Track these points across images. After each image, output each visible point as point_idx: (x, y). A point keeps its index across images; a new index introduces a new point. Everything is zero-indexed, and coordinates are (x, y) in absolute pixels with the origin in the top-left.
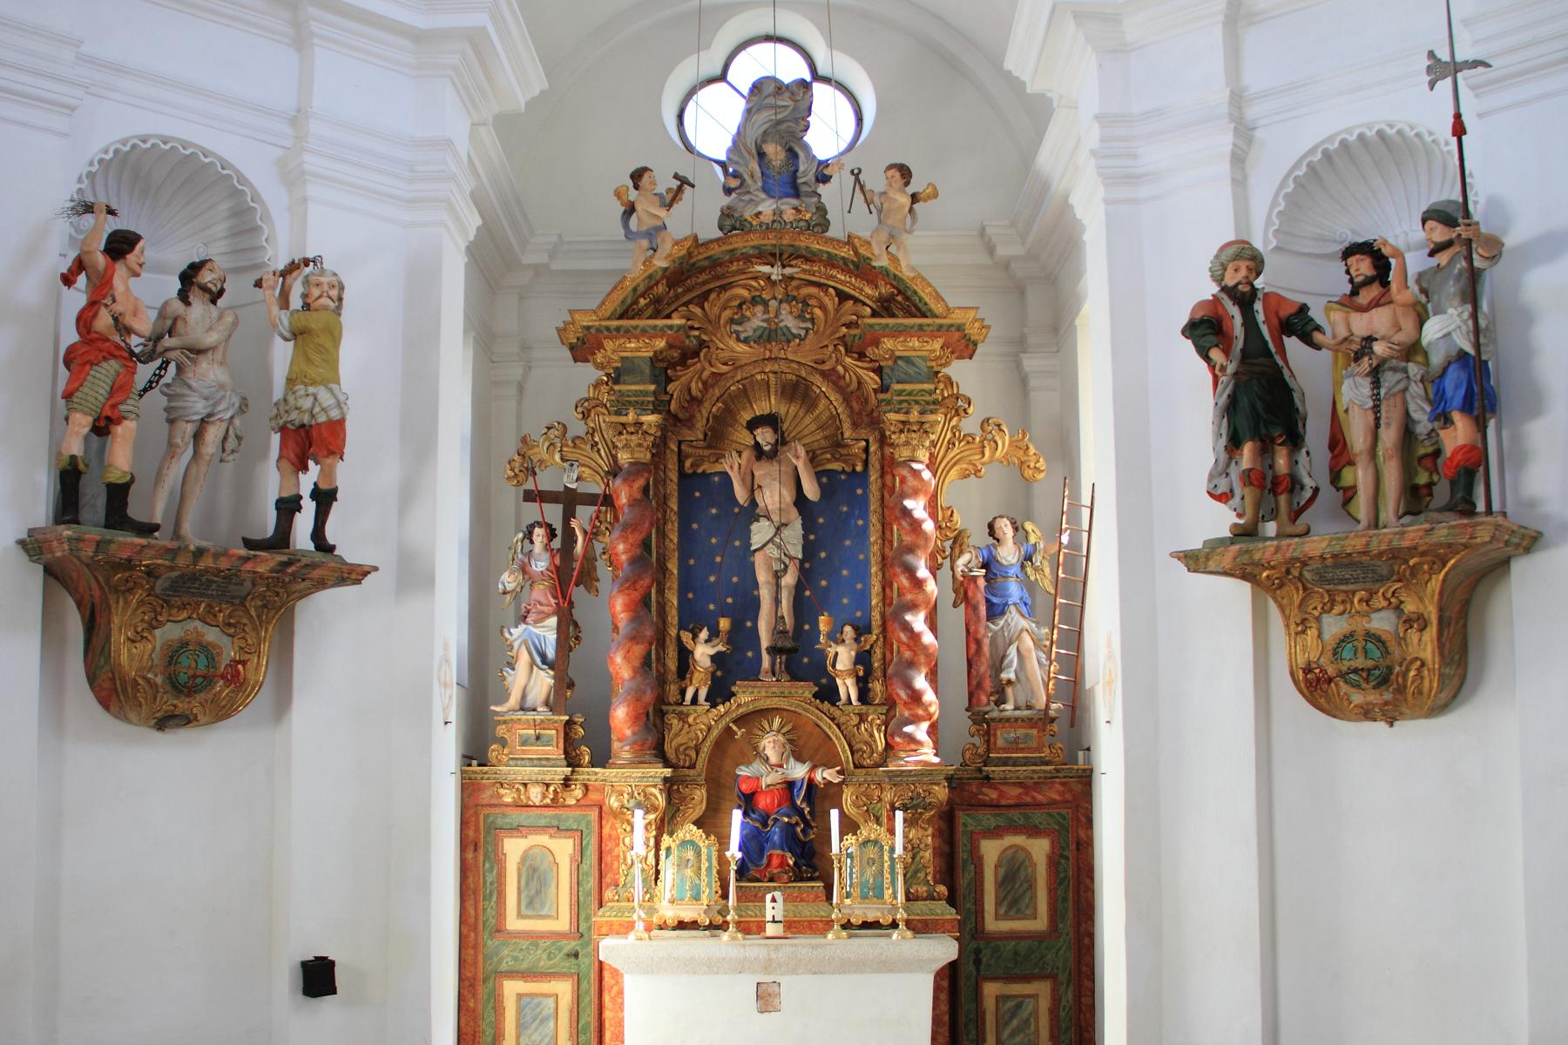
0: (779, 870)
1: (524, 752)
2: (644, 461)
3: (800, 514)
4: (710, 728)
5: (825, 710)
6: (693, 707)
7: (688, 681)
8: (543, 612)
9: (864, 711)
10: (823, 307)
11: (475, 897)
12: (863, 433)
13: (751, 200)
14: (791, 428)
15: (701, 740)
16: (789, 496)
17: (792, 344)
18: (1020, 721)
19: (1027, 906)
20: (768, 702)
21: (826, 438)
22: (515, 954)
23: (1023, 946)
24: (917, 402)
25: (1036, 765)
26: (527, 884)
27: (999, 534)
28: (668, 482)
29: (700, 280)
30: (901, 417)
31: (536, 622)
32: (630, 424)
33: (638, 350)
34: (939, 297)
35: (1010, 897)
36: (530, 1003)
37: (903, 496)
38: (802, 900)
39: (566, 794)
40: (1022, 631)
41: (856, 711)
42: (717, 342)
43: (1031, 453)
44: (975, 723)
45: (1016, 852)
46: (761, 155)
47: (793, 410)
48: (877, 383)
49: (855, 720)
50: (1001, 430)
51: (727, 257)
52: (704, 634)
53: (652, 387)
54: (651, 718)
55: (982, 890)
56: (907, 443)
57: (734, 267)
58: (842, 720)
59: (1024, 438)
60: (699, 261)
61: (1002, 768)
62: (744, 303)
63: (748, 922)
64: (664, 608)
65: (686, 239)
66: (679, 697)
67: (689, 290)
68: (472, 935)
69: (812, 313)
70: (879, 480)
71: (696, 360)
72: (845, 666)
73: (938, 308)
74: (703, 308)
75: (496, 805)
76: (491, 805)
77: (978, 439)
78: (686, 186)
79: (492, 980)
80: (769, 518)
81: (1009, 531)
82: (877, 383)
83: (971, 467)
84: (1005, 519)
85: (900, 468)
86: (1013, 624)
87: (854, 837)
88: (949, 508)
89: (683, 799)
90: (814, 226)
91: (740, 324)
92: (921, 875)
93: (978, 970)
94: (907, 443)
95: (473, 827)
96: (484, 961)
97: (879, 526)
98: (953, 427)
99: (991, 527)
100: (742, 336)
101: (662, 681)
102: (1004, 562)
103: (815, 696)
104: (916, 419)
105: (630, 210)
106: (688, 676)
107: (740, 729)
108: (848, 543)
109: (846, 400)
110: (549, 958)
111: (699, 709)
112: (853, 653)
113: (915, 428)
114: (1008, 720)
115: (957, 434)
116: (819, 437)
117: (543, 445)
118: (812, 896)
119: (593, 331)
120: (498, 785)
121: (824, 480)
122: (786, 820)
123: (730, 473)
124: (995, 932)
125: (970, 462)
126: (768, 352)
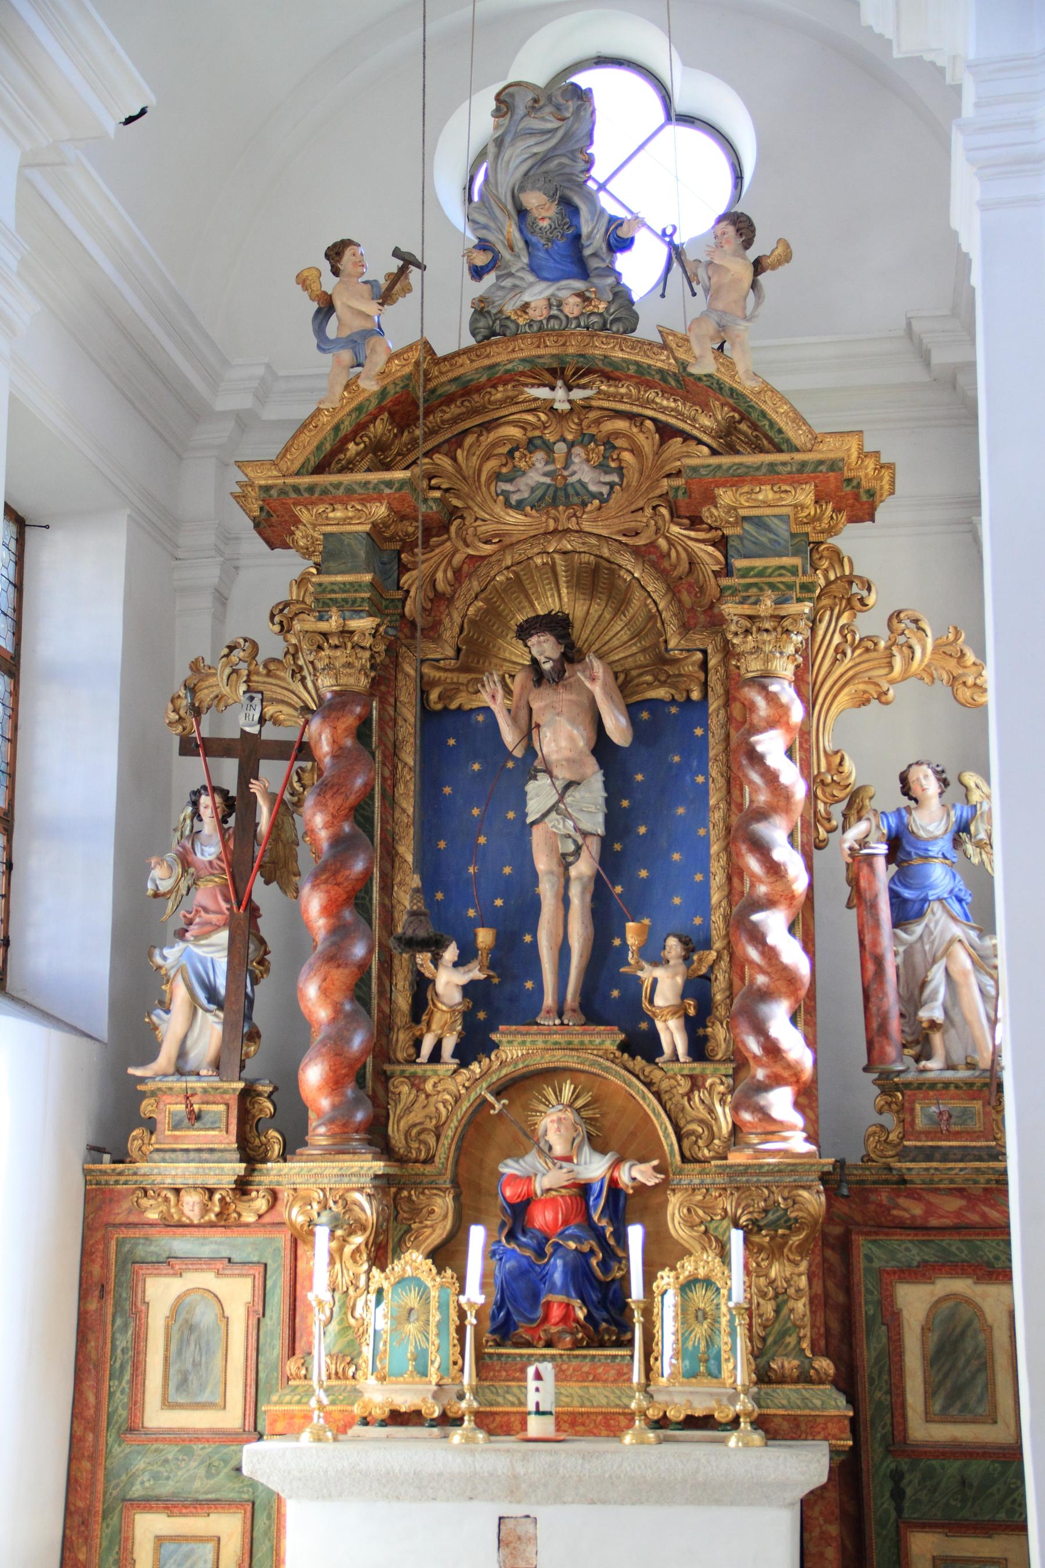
0: (560, 1328)
1: (176, 1137)
2: (356, 689)
3: (601, 767)
4: (458, 1099)
5: (637, 1070)
6: (430, 1067)
7: (423, 1026)
8: (210, 923)
9: (697, 1071)
10: (635, 450)
11: (97, 1372)
12: (698, 639)
13: (515, 286)
14: (593, 638)
15: (443, 1119)
16: (581, 739)
17: (589, 508)
18: (952, 1087)
19: (980, 1401)
20: (548, 1057)
21: (644, 650)
22: (156, 1468)
23: (976, 1469)
24: (773, 586)
25: (980, 1159)
26: (180, 1352)
27: (916, 791)
28: (400, 722)
29: (446, 416)
30: (746, 609)
31: (197, 938)
32: (331, 634)
33: (345, 521)
34: (798, 419)
35: (949, 1384)
36: (174, 1552)
37: (755, 730)
38: (596, 1379)
39: (241, 1207)
40: (951, 942)
41: (686, 1072)
42: (476, 509)
43: (969, 663)
44: (884, 1092)
45: (957, 1305)
46: (522, 213)
47: (596, 609)
48: (718, 562)
49: (685, 1085)
50: (920, 628)
51: (484, 379)
52: (451, 953)
53: (368, 577)
54: (369, 1083)
55: (901, 1370)
56: (757, 650)
57: (499, 395)
58: (665, 1085)
59: (956, 639)
60: (443, 384)
61: (924, 1165)
62: (517, 448)
63: (507, 1413)
64: (392, 913)
65: (410, 348)
66: (412, 1051)
67: (431, 433)
68: (90, 1437)
69: (619, 459)
70: (722, 712)
71: (446, 536)
72: (666, 999)
73: (797, 435)
74: (454, 459)
75: (135, 1225)
76: (129, 1225)
77: (882, 644)
78: (412, 267)
79: (117, 1512)
80: (548, 772)
81: (931, 786)
82: (718, 562)
83: (872, 690)
84: (925, 767)
85: (746, 689)
86: (937, 932)
87: (672, 1274)
88: (836, 753)
89: (416, 1212)
90: (613, 321)
91: (510, 480)
92: (792, 1340)
93: (899, 1510)
94: (757, 650)
95: (99, 1261)
96: (107, 1481)
97: (721, 782)
98: (843, 627)
99: (904, 779)
100: (514, 499)
101: (385, 1027)
102: (922, 834)
103: (623, 1047)
104: (770, 612)
105: (326, 308)
106: (424, 1017)
107: (498, 1101)
108: (681, 811)
109: (672, 591)
110: (209, 1475)
111: (439, 1067)
112: (679, 980)
113: (767, 625)
114: (932, 1085)
115: (849, 637)
116: (634, 649)
117: (222, 672)
118: (613, 1373)
119: (274, 493)
120: (140, 1193)
121: (645, 715)
122: (572, 1245)
123: (493, 707)
124: (925, 1444)
125: (871, 681)
126: (551, 522)
